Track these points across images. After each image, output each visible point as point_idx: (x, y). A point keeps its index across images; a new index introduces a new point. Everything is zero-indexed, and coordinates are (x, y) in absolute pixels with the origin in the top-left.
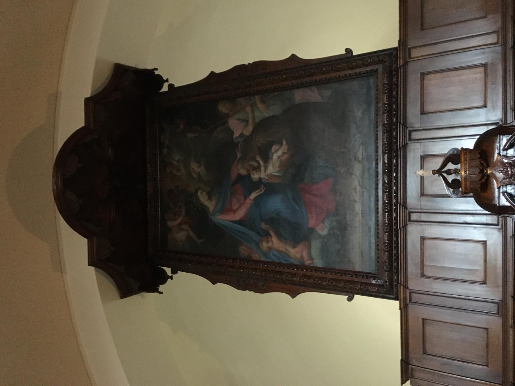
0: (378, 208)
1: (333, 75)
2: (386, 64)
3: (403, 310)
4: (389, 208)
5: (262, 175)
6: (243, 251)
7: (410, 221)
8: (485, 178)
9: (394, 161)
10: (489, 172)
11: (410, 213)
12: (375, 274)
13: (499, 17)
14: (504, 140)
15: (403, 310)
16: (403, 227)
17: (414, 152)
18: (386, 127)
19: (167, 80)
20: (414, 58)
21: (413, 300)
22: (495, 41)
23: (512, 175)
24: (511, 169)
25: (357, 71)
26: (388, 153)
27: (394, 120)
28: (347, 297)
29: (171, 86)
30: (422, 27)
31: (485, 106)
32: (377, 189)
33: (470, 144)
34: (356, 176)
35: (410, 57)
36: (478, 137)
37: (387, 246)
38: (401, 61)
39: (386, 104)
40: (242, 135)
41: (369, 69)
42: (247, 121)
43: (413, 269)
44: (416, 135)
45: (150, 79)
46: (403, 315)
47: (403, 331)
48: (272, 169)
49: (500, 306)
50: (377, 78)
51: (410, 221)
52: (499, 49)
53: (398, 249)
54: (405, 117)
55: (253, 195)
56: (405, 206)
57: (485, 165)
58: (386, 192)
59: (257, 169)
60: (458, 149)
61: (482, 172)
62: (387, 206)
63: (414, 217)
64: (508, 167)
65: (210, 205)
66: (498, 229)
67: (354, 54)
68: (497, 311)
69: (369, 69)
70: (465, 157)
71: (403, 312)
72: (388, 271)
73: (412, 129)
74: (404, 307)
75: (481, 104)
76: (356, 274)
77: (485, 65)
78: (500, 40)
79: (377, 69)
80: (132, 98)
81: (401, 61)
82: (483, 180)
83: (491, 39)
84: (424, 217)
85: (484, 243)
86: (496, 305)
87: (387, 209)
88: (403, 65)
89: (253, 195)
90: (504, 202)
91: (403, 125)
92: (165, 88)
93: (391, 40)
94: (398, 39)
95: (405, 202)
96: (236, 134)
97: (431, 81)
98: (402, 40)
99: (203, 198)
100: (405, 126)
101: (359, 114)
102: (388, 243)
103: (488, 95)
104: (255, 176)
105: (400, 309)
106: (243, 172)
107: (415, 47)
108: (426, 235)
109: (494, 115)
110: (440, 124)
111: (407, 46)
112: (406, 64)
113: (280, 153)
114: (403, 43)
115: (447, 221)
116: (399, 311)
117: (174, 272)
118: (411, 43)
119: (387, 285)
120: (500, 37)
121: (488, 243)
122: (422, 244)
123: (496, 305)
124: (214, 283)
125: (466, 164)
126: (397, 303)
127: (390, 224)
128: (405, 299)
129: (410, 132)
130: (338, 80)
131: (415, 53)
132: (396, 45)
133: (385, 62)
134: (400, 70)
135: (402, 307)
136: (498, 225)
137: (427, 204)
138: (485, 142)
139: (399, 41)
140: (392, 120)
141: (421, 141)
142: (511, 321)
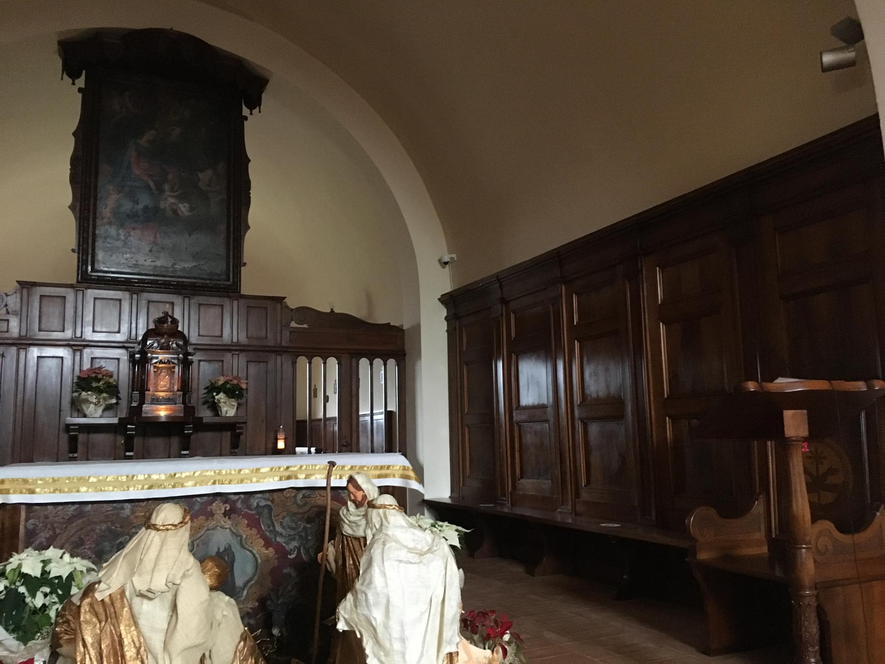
1: (231, 254)
5: (167, 193)
6: (105, 168)
14: (181, 343)
17: (177, 300)
19: (251, 114)
22: (81, 293)
29: (246, 118)
31: (199, 335)
40: (199, 179)
42: (209, 186)
44: (187, 300)
45: (255, 103)
48: (168, 201)
55: (152, 185)
59: (172, 190)
63: (135, 296)
65: (144, 141)
75: (117, 330)
77: (221, 336)
80: (242, 87)
83: (235, 340)
84: (134, 302)
85: (94, 331)
89: (152, 185)
90: (148, 342)
92: (246, 111)
93: (245, 290)
96: (200, 175)
97: (217, 310)
99: (149, 136)
103: (834, 72)
104: (167, 187)
106: (170, 177)
108: (123, 302)
109: (194, 339)
110: (192, 312)
113: (183, 209)
117: (80, 90)
118: (242, 301)
124: (74, 134)
130: (228, 257)
131: (235, 302)
137: (144, 303)
138: (181, 335)
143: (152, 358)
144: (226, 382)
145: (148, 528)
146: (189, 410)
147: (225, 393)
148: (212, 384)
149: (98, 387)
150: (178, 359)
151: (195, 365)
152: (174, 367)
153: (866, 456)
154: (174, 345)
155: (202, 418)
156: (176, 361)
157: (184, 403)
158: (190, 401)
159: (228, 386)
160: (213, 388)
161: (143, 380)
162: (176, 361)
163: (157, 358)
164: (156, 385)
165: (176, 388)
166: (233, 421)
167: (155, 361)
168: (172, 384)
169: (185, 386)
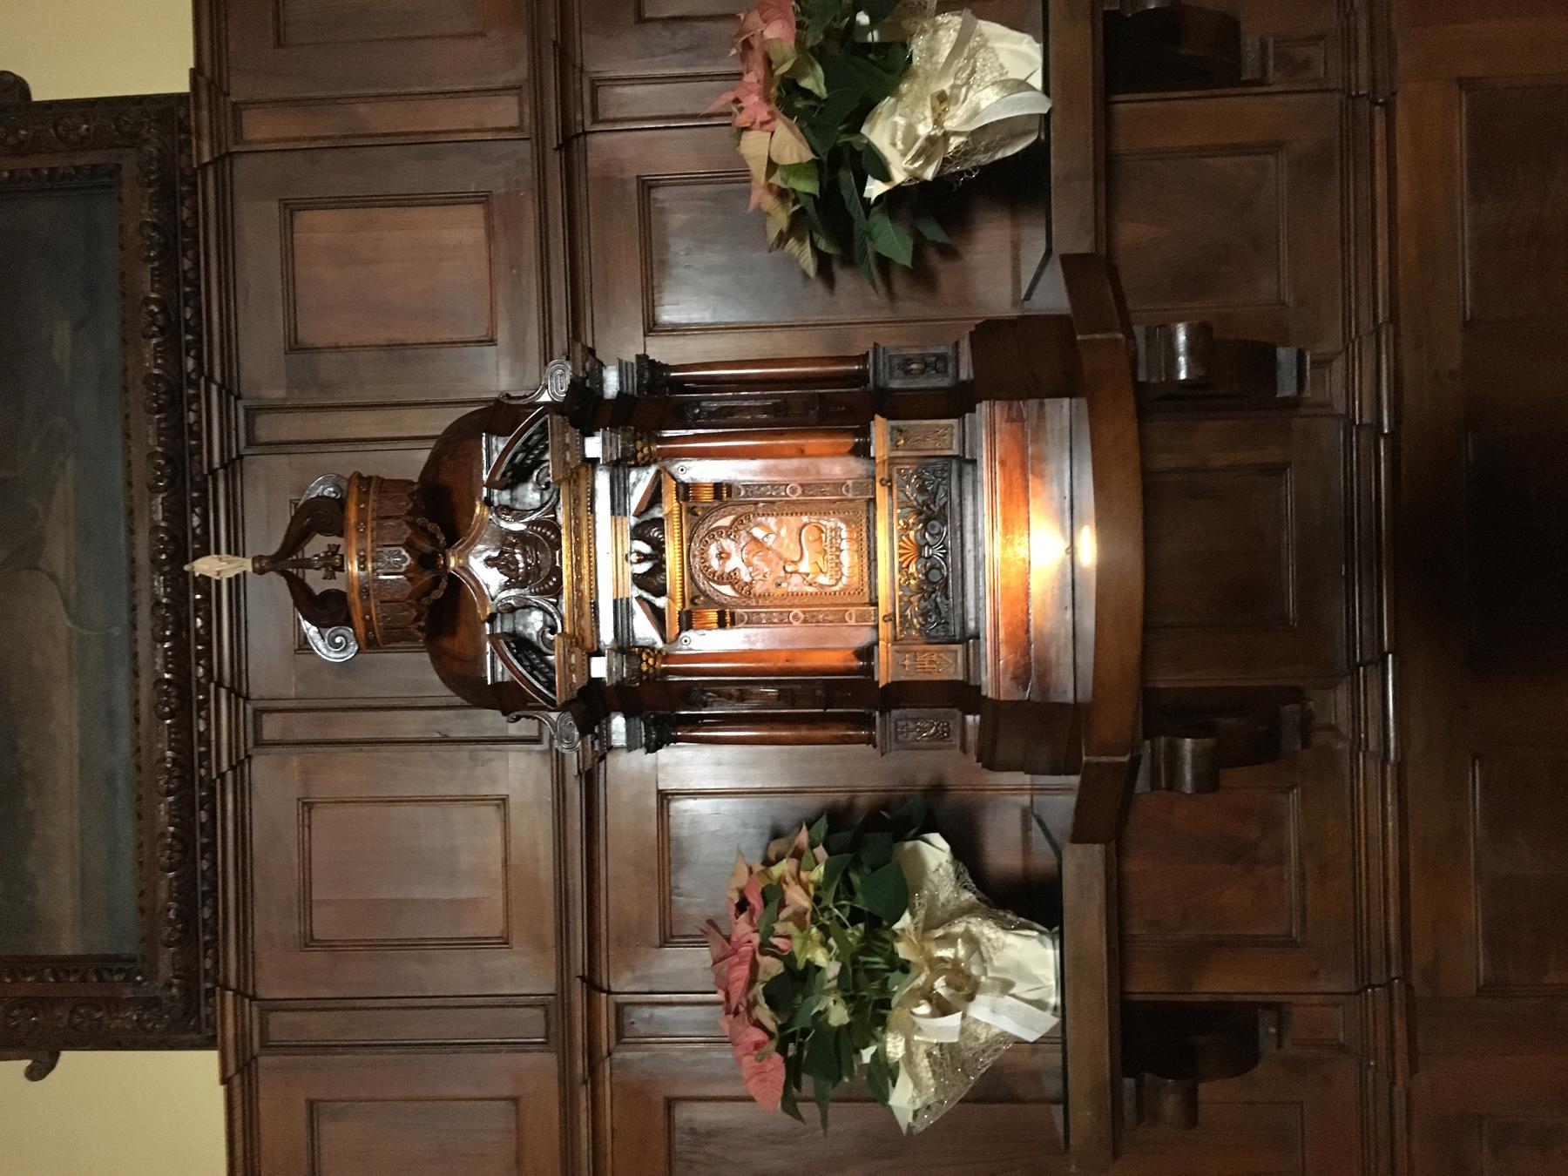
0: (137, 703)
1: (1371, 1088)
2: (146, 148)
3: (237, 1081)
4: (183, 699)
7: (259, 743)
8: (444, 584)
9: (196, 521)
10: (452, 564)
11: (258, 713)
12: (131, 960)
13: (521, 41)
15: (237, 1081)
16: (232, 768)
18: (156, 389)
20: (250, 142)
21: (276, 1035)
23: (527, 574)
24: (524, 555)
25: (43, 163)
26: (165, 489)
27: (190, 364)
28: (28, 1062)
30: (278, 33)
32: (134, 627)
33: (411, 464)
34: (52, 577)
35: (238, 137)
36: (432, 444)
37: (170, 846)
38: (206, 147)
39: (155, 301)
41: (85, 159)
43: (272, 920)
46: (238, 1100)
47: (239, 1162)
49: (552, 1015)
50: (120, 199)
51: (259, 743)
52: (525, 149)
53: (216, 852)
54: (230, 358)
56: (238, 693)
57: (442, 538)
58: (164, 639)
60: (411, 483)
61: (427, 561)
62: (166, 693)
64: (513, 546)
66: (540, 752)
67: (36, 97)
68: (542, 1031)
69: (85, 159)
70: (360, 510)
71: (237, 1091)
72: (177, 943)
73: (254, 403)
74: (239, 1070)
76: (63, 966)
78: (527, 121)
79: (119, 166)
81: (206, 147)
82: (438, 594)
86: (539, 1013)
87: (167, 704)
88: (214, 162)
91: (221, 387)
94: (190, 63)
95: (239, 672)
98: (207, 72)
100: (229, 391)
101: (62, 335)
102: (173, 835)
105: (225, 1080)
107: (254, 103)
111: (227, 94)
112: (222, 160)
114: (211, 83)
115: (382, 736)
116: (220, 1090)
118: (240, 89)
119: (172, 998)
120: (527, 110)
121: (512, 802)
122: (306, 825)
123: (539, 1013)
125: (362, 536)
126: (212, 1057)
127: (185, 763)
128: (242, 1038)
129: (251, 413)
131: (259, 128)
132: (180, 84)
133: (146, 141)
134: (204, 181)
135: (232, 1068)
136: (538, 741)
139: (195, 74)
140: (180, 363)
141: (293, 449)
142: (580, 1062)
143: (625, 647)
144: (787, 96)
145: (614, 752)
146: (1018, 366)
147: (864, 110)
148: (798, 226)
149: (849, 988)
150: (620, 466)
151: (662, 351)
152: (686, 491)
153: (816, 369)
154: (530, 495)
155: (973, 411)
156: (640, 482)
157: (957, 402)
158: (936, 364)
159: (815, 81)
160: (830, 209)
161: (789, 694)
162: (640, 482)
163: (622, 610)
164: (819, 608)
165: (839, 468)
166: (1081, 41)
167: (644, 629)
168: (811, 499)
169: (820, 403)
